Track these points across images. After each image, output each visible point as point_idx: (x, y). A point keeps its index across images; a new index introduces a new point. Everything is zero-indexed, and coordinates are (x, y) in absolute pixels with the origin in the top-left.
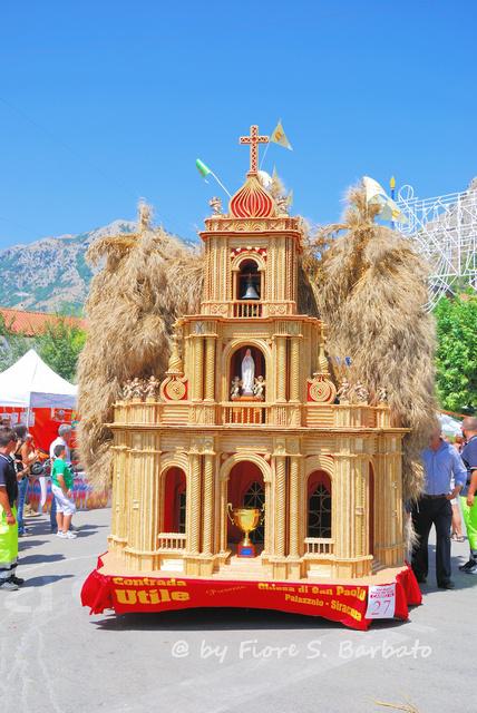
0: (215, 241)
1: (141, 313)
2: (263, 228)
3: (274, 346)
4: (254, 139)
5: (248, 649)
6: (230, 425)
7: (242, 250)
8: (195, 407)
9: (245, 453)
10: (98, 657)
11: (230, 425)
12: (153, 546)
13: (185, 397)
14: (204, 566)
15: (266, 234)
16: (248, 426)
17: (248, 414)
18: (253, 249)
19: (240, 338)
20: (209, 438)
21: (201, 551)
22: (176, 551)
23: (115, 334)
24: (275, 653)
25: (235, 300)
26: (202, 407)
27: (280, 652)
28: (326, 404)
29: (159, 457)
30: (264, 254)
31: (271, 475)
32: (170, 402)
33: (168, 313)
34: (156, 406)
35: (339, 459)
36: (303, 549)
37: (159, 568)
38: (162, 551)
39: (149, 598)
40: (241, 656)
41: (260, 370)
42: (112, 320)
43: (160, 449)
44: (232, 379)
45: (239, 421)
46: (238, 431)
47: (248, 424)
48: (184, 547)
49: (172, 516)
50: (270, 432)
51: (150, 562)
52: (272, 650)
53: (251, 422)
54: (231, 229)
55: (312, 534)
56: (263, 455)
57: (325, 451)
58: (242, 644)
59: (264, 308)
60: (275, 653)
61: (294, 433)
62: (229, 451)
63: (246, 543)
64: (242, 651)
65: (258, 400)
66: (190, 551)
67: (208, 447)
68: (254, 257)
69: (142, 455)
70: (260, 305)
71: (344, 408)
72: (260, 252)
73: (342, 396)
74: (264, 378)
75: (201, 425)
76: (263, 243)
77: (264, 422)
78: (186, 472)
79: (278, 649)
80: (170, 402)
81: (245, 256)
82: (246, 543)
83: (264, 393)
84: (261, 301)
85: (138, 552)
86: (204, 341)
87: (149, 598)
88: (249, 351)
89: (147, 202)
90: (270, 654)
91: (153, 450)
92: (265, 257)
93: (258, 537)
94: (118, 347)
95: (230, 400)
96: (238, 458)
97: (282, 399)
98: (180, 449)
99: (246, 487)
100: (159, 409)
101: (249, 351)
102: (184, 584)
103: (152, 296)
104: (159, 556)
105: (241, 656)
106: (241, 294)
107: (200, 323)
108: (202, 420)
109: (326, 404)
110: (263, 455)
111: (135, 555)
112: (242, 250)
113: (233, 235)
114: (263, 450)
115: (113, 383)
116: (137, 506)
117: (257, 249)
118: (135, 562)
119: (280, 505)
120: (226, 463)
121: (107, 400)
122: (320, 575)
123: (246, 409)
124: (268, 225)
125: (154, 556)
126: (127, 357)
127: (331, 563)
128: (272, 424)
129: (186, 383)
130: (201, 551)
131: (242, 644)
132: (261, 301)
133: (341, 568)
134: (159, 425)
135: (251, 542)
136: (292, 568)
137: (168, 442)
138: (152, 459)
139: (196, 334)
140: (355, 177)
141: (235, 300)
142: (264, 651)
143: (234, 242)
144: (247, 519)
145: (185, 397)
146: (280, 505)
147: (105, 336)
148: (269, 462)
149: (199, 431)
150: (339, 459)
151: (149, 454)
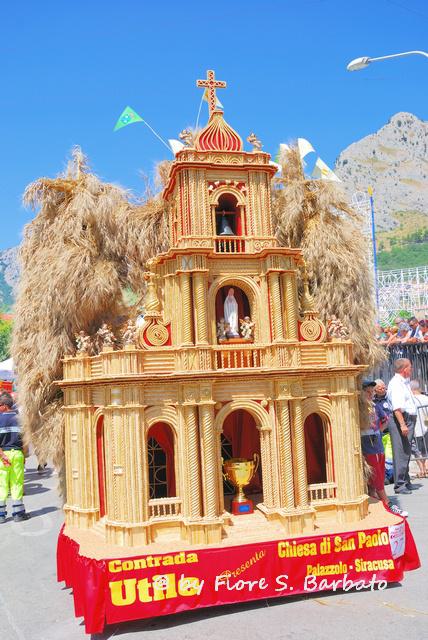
0: (191, 174)
1: (94, 259)
2: (241, 162)
3: (264, 284)
4: (212, 83)
5: (223, 583)
6: (223, 370)
7: (221, 184)
8: (188, 351)
9: (241, 401)
10: (44, 579)
11: (223, 370)
12: (144, 516)
13: (168, 343)
14: (211, 533)
15: (245, 169)
16: (242, 370)
17: (238, 357)
18: (232, 184)
19: (226, 276)
20: (207, 385)
21: (202, 514)
22: (170, 518)
23: (65, 280)
24: (247, 586)
25: (215, 236)
26: (196, 351)
27: (251, 585)
28: (316, 343)
29: (146, 410)
30: (243, 188)
31: (267, 421)
32: (151, 349)
33: (119, 259)
34: (138, 354)
35: (337, 399)
36: (311, 496)
37: (153, 541)
38: (154, 520)
39: (151, 592)
40: (217, 589)
41: (245, 310)
42: (62, 265)
43: (145, 403)
44: (218, 321)
45: (232, 366)
46: (235, 376)
47: (242, 368)
48: (179, 512)
49: (161, 480)
50: (271, 375)
51: (143, 535)
52: (244, 583)
53: (245, 366)
54: (208, 161)
55: (311, 480)
56: (259, 401)
57: (322, 392)
58: (218, 578)
59: (246, 243)
60: (247, 586)
61: (298, 373)
62: (223, 399)
63: (241, 499)
64: (217, 584)
65: (248, 342)
66: (188, 517)
67: (207, 397)
68: (233, 191)
69: (122, 411)
70: (243, 241)
71: (337, 346)
72: (239, 186)
73: (334, 334)
74: (250, 319)
75: (196, 371)
76: (242, 177)
77: (259, 365)
78: (157, 420)
79: (249, 582)
80: (151, 349)
81: (224, 190)
82: (241, 499)
83: (252, 336)
84: (243, 236)
85: (127, 526)
86: (191, 277)
87: (151, 592)
88: (232, 291)
89: (82, 151)
90: (242, 586)
91: (138, 405)
92: (244, 192)
93: (255, 491)
94: (71, 293)
95: (219, 343)
96: (234, 406)
97: (188, 343)
98: (168, 402)
99: (239, 437)
100: (141, 357)
101: (232, 291)
102: (194, 558)
103: (101, 238)
104: (151, 526)
105: (217, 589)
106: (219, 230)
107: (186, 257)
108: (196, 365)
109: (316, 343)
110: (259, 401)
111: (124, 529)
112: (221, 184)
113: (211, 167)
114: (259, 396)
115: (61, 337)
116: (120, 471)
117: (236, 183)
118: (122, 537)
119: (280, 448)
120: (221, 411)
121: (55, 355)
122: (331, 524)
123: (232, 353)
124: (245, 160)
125: (146, 528)
126: (78, 306)
127: (334, 507)
128: (269, 364)
129: (168, 327)
130: (202, 514)
131: (218, 578)
132: (243, 236)
133: (348, 512)
134: (141, 375)
135: (246, 497)
136: (306, 520)
137: (154, 394)
138: (137, 416)
139: (184, 268)
140: (292, 136)
141: (215, 236)
142: (237, 585)
143: (212, 175)
144: (242, 473)
145: (168, 343)
146: (280, 448)
147: (53, 282)
148: (267, 408)
149: (196, 378)
150: (337, 399)
151: (133, 410)
